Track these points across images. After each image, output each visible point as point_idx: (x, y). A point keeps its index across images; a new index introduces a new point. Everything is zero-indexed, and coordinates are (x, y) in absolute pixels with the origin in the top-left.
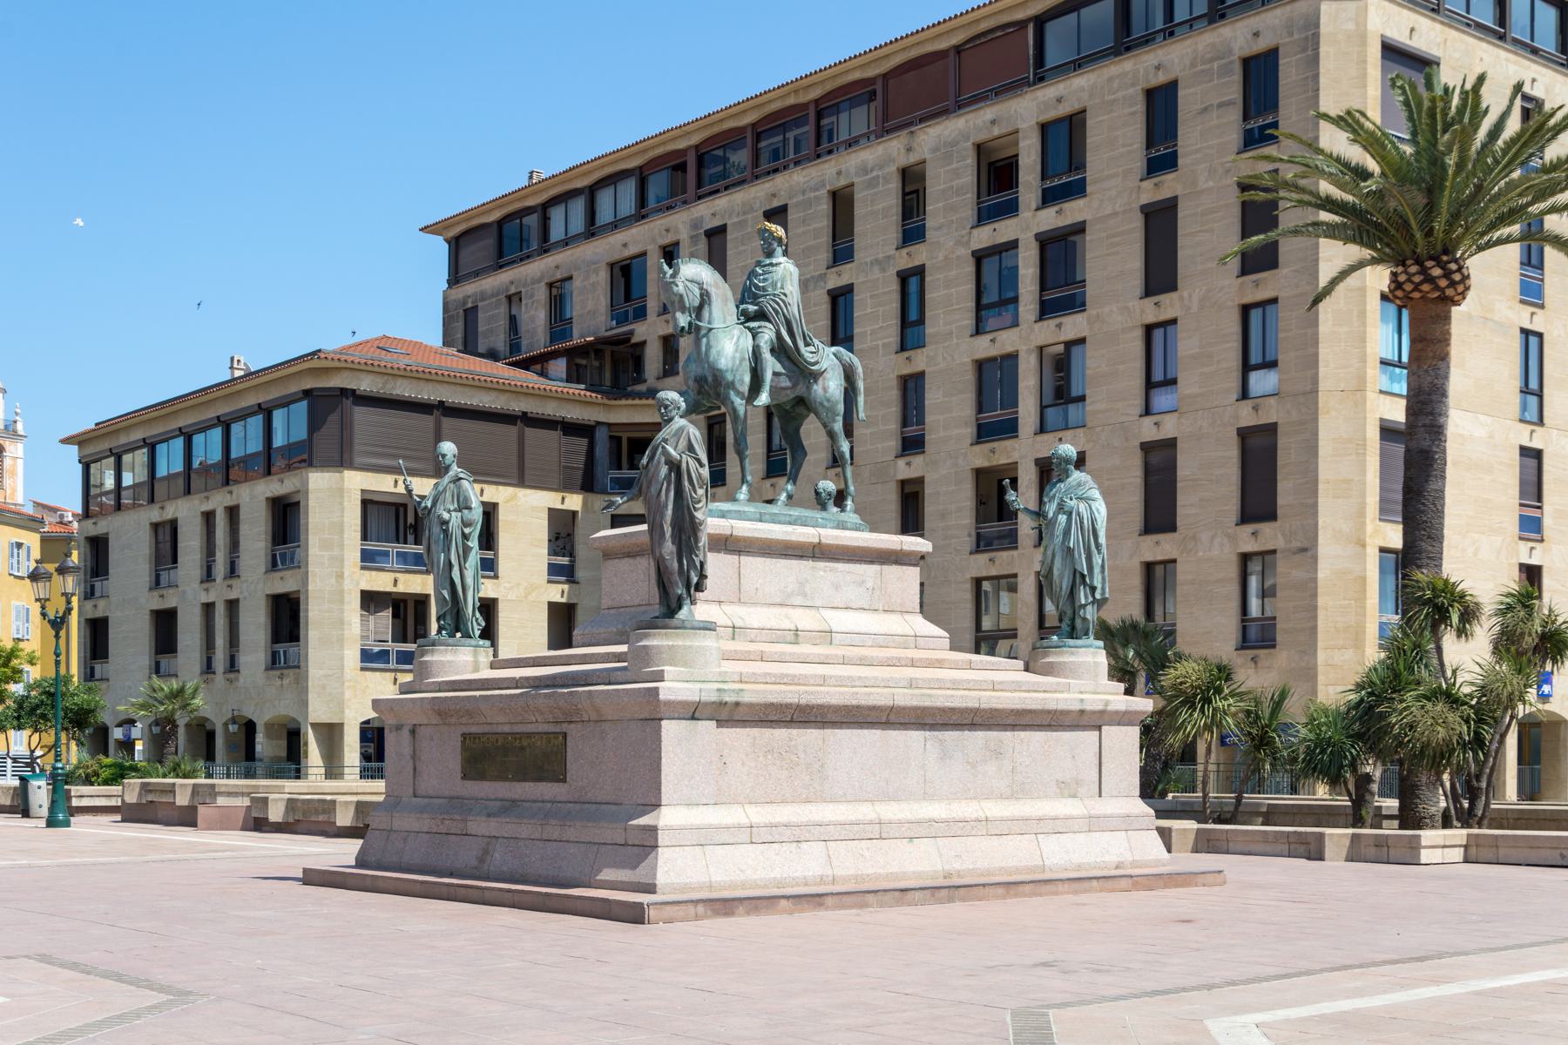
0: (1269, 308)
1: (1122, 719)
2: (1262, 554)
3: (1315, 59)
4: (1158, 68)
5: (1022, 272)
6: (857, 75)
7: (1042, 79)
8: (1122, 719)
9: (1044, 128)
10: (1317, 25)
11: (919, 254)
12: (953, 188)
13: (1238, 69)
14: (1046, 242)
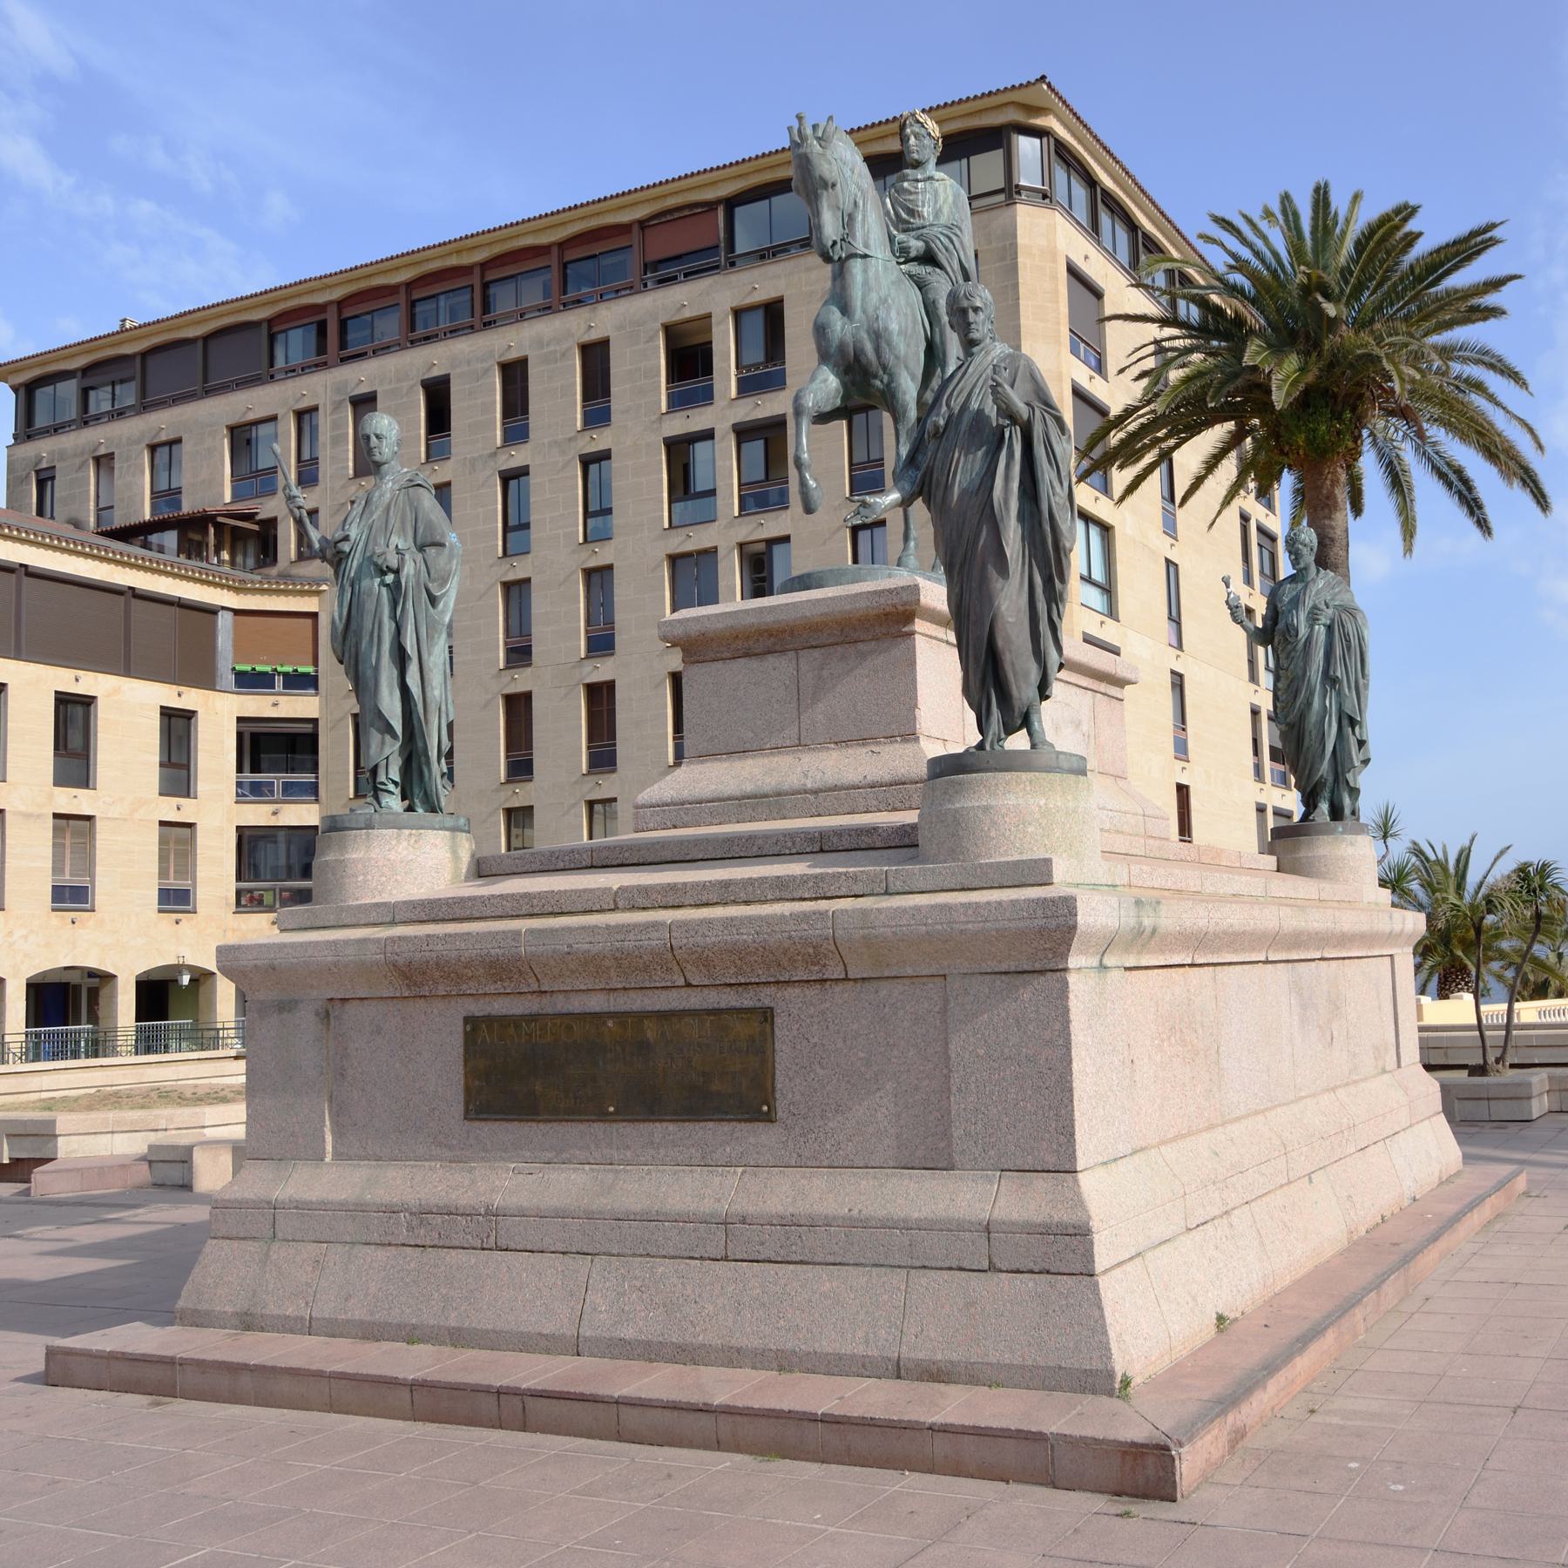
3: (1014, 269)
7: (733, 264)
10: (1015, 236)
12: (642, 371)
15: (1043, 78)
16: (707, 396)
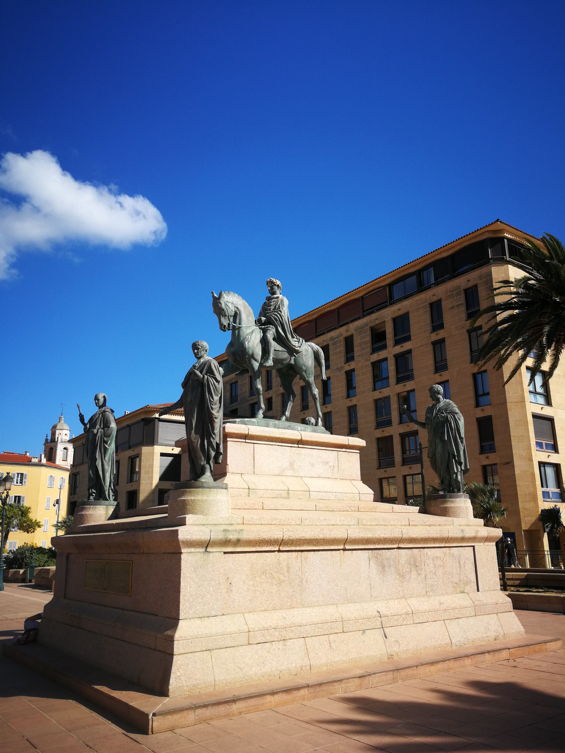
0: (483, 374)
1: (487, 539)
2: (491, 465)
4: (434, 295)
5: (389, 368)
6: (329, 309)
8: (487, 539)
9: (395, 320)
11: (353, 365)
12: (363, 342)
13: (463, 293)
14: (397, 357)
15: (498, 220)
16: (384, 347)
